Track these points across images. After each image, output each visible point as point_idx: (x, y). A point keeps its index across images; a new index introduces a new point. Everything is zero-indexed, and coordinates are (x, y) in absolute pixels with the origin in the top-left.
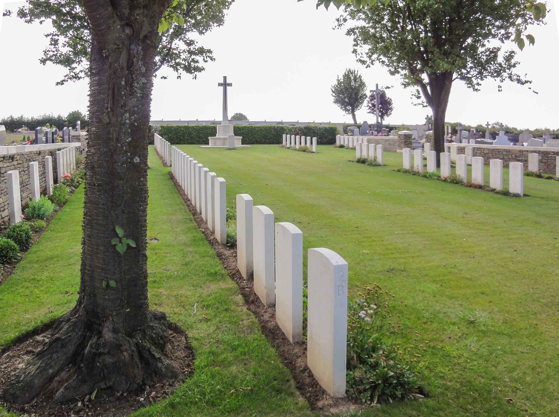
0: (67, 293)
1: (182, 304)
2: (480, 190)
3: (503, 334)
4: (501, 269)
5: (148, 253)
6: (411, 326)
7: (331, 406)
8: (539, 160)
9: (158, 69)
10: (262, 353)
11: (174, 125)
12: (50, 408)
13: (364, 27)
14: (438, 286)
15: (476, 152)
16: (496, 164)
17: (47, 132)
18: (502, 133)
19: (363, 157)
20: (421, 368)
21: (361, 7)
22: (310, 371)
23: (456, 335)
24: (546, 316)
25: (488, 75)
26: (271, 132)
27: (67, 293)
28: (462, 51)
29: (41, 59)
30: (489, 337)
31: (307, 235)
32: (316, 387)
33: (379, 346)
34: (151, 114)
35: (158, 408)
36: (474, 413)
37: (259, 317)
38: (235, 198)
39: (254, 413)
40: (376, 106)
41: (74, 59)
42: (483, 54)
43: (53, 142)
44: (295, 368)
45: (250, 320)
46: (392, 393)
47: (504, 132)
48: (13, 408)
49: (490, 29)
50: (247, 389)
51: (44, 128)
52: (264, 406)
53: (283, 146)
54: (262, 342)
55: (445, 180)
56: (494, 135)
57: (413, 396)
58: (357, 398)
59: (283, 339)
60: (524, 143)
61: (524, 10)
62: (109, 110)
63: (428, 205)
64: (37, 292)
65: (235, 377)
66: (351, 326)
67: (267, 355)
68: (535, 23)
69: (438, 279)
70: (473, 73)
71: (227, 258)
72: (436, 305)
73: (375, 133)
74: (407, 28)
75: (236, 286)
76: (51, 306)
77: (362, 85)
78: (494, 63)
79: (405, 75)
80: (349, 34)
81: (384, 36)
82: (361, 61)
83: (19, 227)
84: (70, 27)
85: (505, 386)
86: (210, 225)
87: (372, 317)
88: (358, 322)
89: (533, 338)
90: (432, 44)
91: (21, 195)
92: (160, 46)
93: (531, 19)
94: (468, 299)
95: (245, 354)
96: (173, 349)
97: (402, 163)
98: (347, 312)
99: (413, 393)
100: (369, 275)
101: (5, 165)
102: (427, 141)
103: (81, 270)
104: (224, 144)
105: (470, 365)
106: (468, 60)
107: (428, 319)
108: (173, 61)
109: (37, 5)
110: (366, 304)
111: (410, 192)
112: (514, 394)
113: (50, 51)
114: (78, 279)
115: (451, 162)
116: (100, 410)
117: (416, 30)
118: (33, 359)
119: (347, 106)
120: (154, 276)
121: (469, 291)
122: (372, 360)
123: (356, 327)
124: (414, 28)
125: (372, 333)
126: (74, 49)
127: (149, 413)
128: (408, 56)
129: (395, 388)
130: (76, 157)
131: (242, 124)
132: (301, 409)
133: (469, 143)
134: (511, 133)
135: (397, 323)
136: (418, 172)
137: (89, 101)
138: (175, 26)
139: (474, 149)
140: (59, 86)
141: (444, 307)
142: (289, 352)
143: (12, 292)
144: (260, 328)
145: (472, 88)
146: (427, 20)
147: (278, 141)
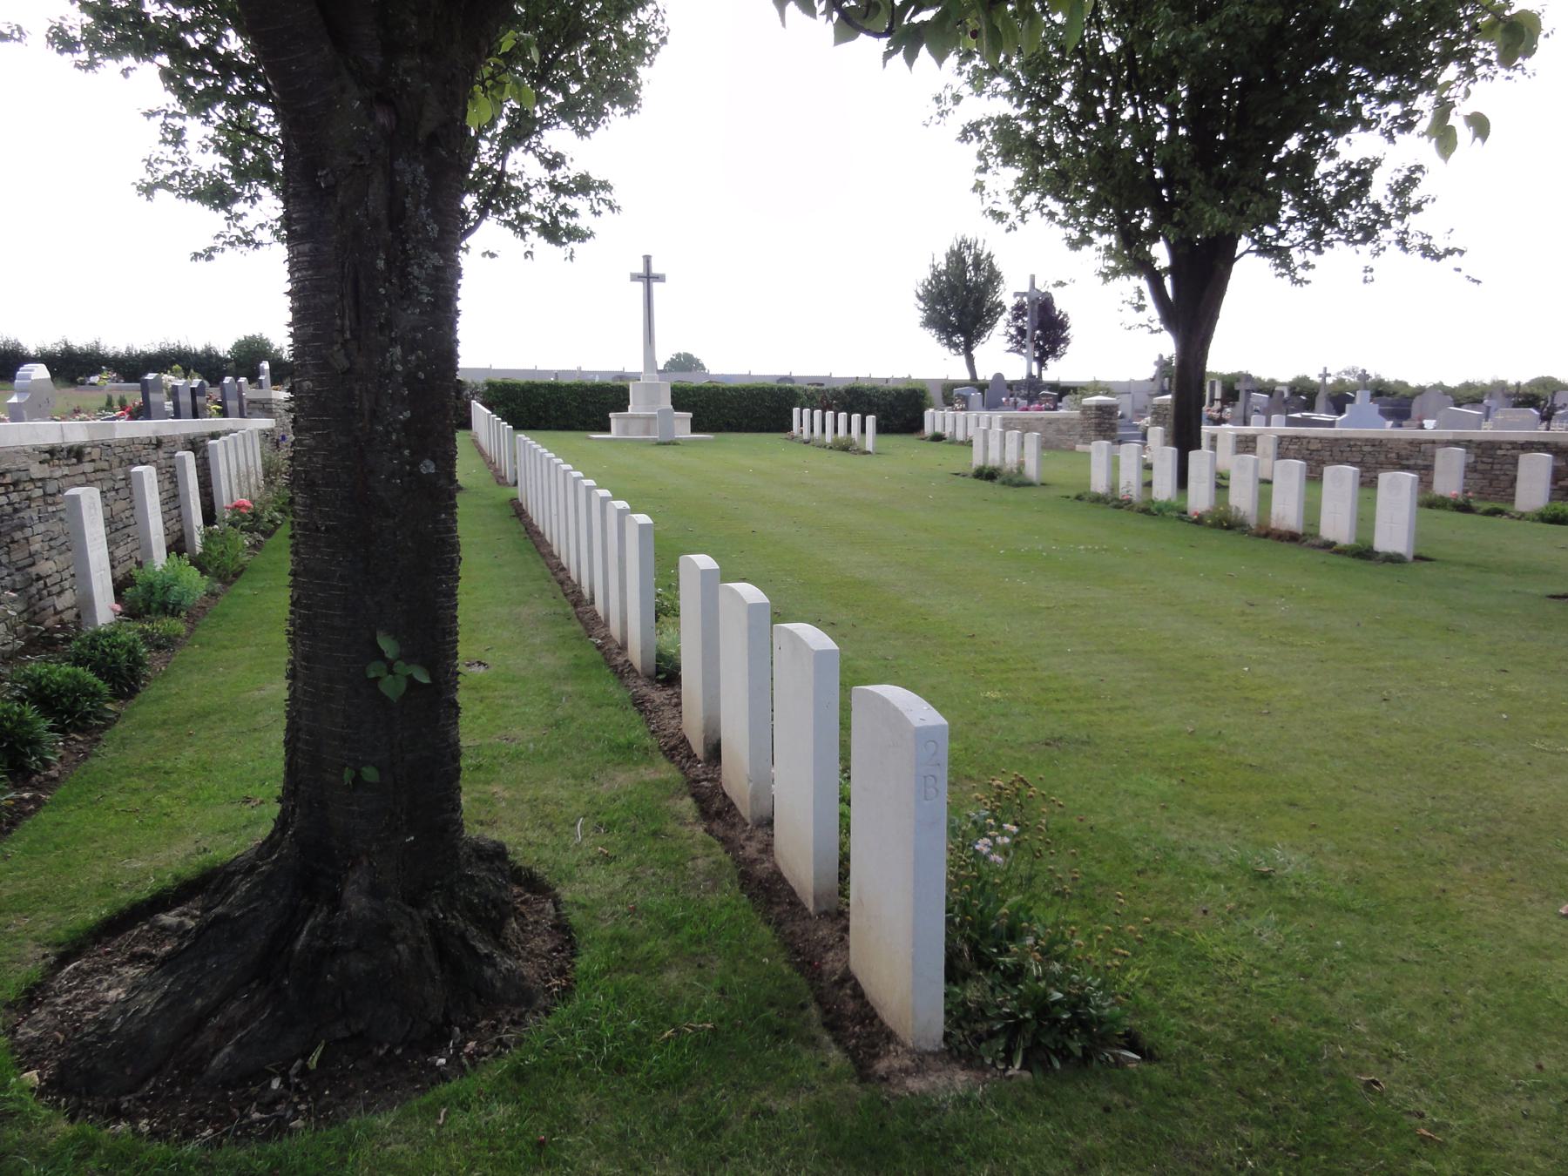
0: (247, 800)
1: (547, 821)
2: (1293, 544)
3: (1349, 910)
4: (1345, 745)
5: (462, 697)
6: (1105, 880)
7: (907, 1071)
8: (1467, 466)
9: (471, 230)
10: (741, 939)
11: (522, 380)
12: (192, 1101)
13: (1007, 118)
14: (1174, 782)
15: (1285, 448)
16: (1341, 479)
17: (175, 387)
18: (1362, 397)
19: (990, 464)
20: (1130, 984)
21: (1001, 59)
22: (857, 985)
23: (1222, 905)
24: (1473, 869)
25: (1338, 239)
26: (763, 400)
27: (247, 800)
28: (1270, 175)
29: (139, 183)
30: (1312, 915)
31: (849, 654)
32: (871, 1024)
33: (1025, 924)
34: (461, 350)
35: (483, 1081)
36: (1275, 1108)
37: (734, 850)
38: (677, 565)
39: (720, 1088)
40: (1029, 334)
41: (238, 190)
42: (1329, 179)
43: (195, 415)
44: (820, 975)
45: (711, 859)
46: (1060, 1046)
47: (1368, 393)
48: (87, 1108)
49: (1357, 104)
50: (703, 1029)
51: (165, 377)
52: (745, 1069)
53: (793, 438)
54: (740, 911)
55: (1199, 521)
56: (1339, 400)
57: (1112, 1054)
58: (971, 1053)
59: (791, 903)
60: (1425, 422)
61: (1468, 40)
62: (348, 335)
63: (1152, 581)
64: (164, 801)
65: (676, 999)
66: (956, 876)
67: (752, 943)
68: (1497, 77)
69: (1173, 765)
70: (1296, 234)
71: (656, 710)
72: (1168, 830)
73: (1023, 403)
74: (1123, 117)
75: (679, 775)
76: (204, 837)
77: (994, 277)
78: (1359, 204)
79: (1109, 247)
80: (966, 139)
81: (1057, 141)
82: (993, 213)
83: (106, 636)
84: (214, 95)
85: (1358, 1046)
86: (615, 629)
87: (1006, 854)
88: (973, 865)
89: (1434, 924)
90: (1186, 159)
91: (111, 553)
92: (475, 166)
93: (1490, 63)
94: (1253, 816)
95: (699, 942)
96: (523, 931)
97: (1089, 477)
98: (945, 839)
99: (1111, 1046)
100: (1000, 752)
101: (58, 474)
102: (1156, 423)
103: (287, 743)
104: (647, 432)
105: (1260, 983)
106: (1284, 200)
107: (1148, 862)
108: (512, 211)
109: (105, 16)
110: (992, 821)
111: (1106, 550)
112: (1384, 1067)
113: (162, 161)
114: (279, 766)
115: (1217, 473)
116: (329, 1095)
117: (1147, 119)
118: (150, 974)
119: (954, 334)
120: (478, 755)
121: (1254, 798)
122: (1007, 960)
123: (967, 877)
124: (1140, 116)
125: (1008, 894)
126: (235, 160)
127: (458, 1096)
128: (1120, 196)
129: (1066, 1030)
130: (262, 456)
131: (693, 380)
132: (833, 1079)
133: (1268, 423)
134: (1389, 395)
135: (1070, 871)
136: (1130, 501)
137: (291, 309)
138: (512, 110)
139: (1281, 439)
140: (202, 262)
141: (1189, 835)
142: (806, 936)
143: (91, 803)
144: (736, 878)
145: (1287, 278)
146: (1179, 88)
147: (783, 425)
